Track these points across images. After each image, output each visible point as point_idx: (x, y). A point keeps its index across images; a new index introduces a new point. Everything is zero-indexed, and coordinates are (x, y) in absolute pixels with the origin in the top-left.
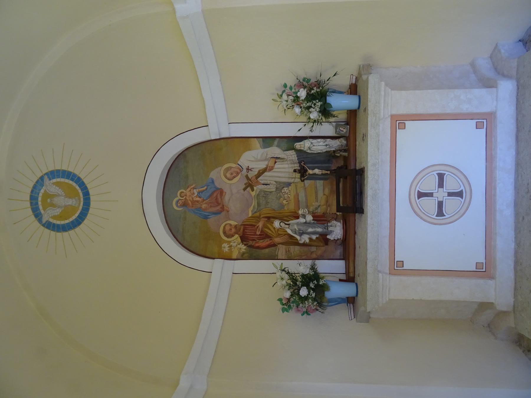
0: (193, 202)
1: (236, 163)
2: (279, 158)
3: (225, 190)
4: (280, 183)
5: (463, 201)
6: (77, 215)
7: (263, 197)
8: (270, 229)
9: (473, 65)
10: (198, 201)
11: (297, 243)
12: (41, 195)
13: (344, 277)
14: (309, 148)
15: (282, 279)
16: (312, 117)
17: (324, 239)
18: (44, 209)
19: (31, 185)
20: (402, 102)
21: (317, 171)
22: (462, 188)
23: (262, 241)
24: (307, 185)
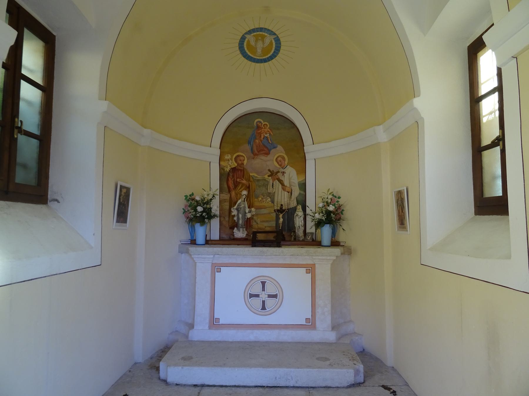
0: (260, 134)
1: (288, 164)
5: (260, 310)
6: (250, 55)
9: (350, 321)
10: (261, 137)
11: (231, 207)
12: (264, 33)
13: (208, 238)
14: (297, 215)
15: (208, 195)
16: (316, 215)
17: (234, 225)
19: (270, 28)
21: (281, 220)
22: (268, 310)
24: (272, 214)
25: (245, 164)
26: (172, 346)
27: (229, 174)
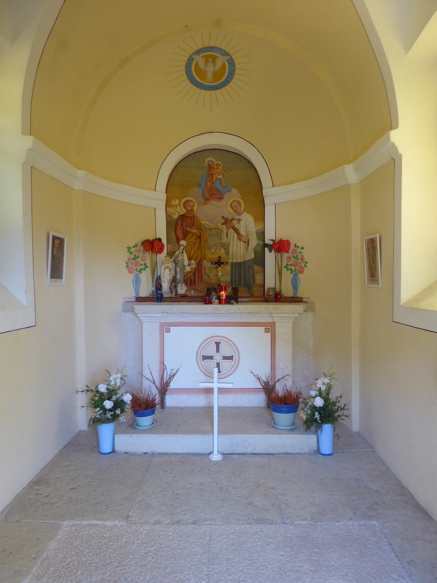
0: (212, 175)
3: (222, 201)
6: (199, 80)
7: (217, 233)
8: (191, 238)
10: (213, 178)
12: (215, 54)
18: (203, 57)
20: (284, 329)
23: (181, 231)
25: (195, 211)
27: (177, 222)
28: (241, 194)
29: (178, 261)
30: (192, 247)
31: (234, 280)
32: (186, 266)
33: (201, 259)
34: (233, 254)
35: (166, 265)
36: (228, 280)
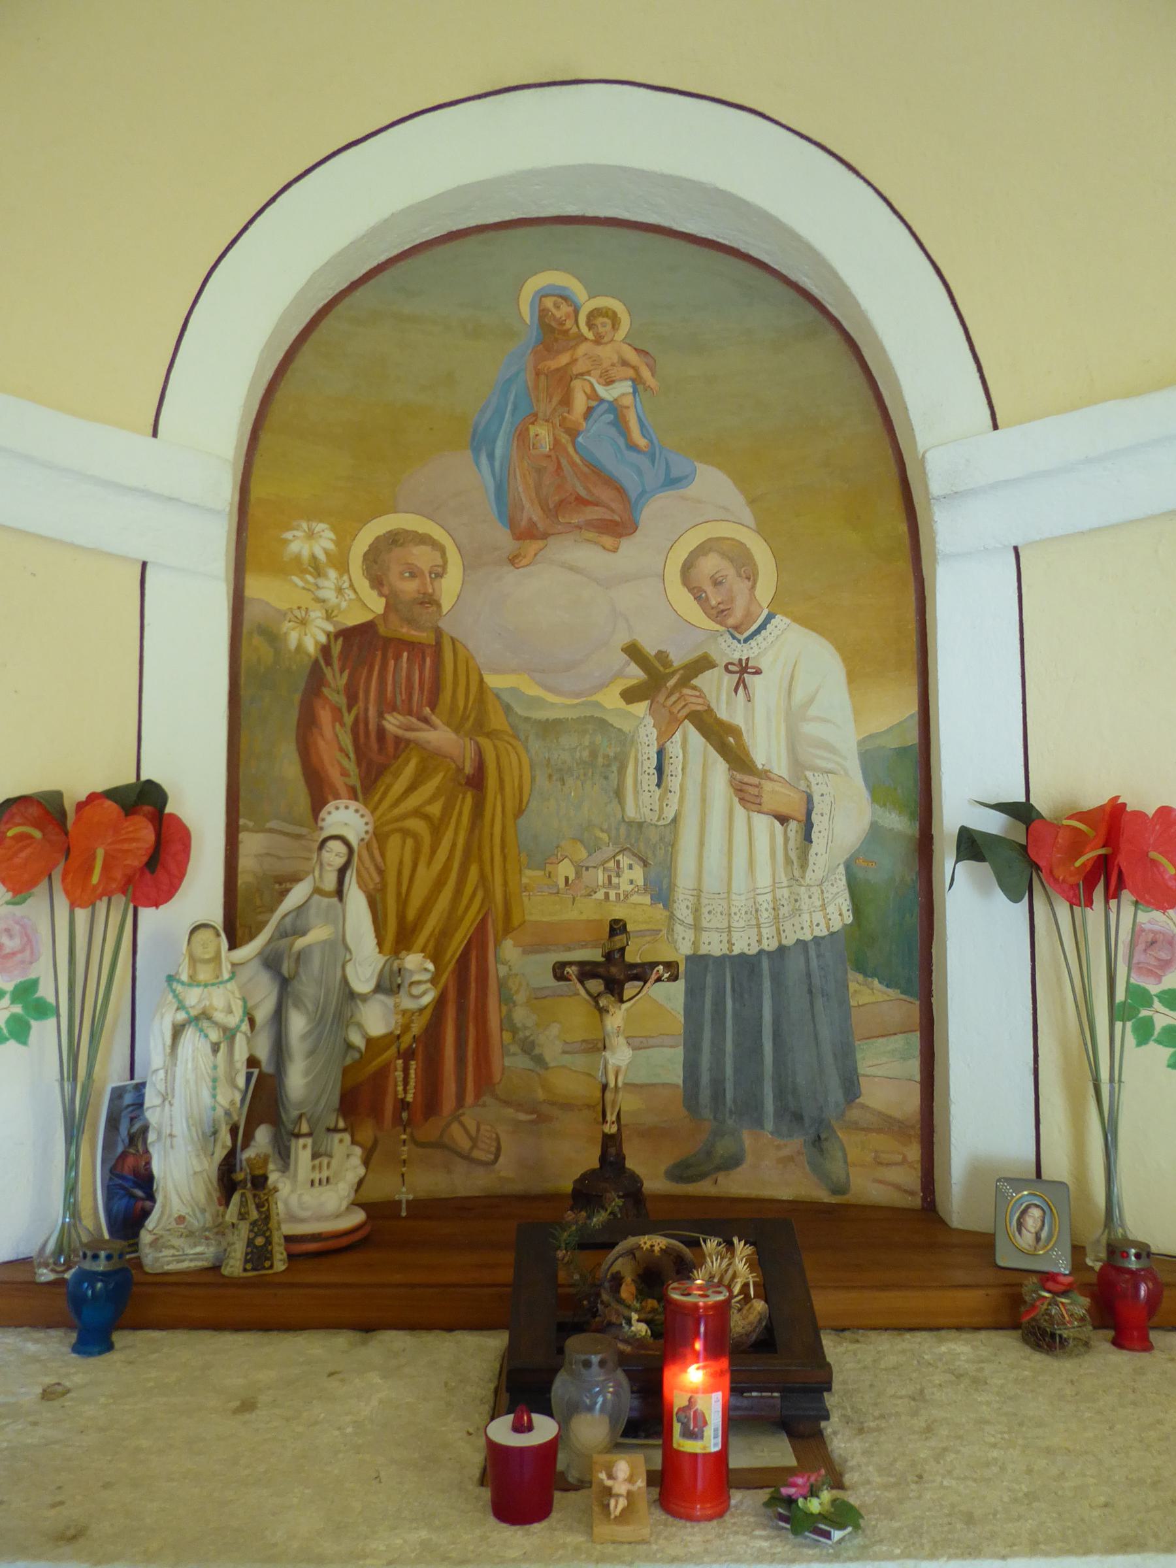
0: (563, 380)
2: (808, 838)
3: (628, 546)
4: (672, 845)
7: (594, 754)
8: (412, 788)
10: (566, 401)
23: (347, 741)
25: (446, 606)
26: (347, 1208)
27: (315, 680)
28: (752, 502)
29: (301, 957)
30: (417, 852)
31: (705, 1079)
32: (364, 998)
33: (481, 928)
34: (698, 892)
35: (193, 997)
36: (888, 1350)
